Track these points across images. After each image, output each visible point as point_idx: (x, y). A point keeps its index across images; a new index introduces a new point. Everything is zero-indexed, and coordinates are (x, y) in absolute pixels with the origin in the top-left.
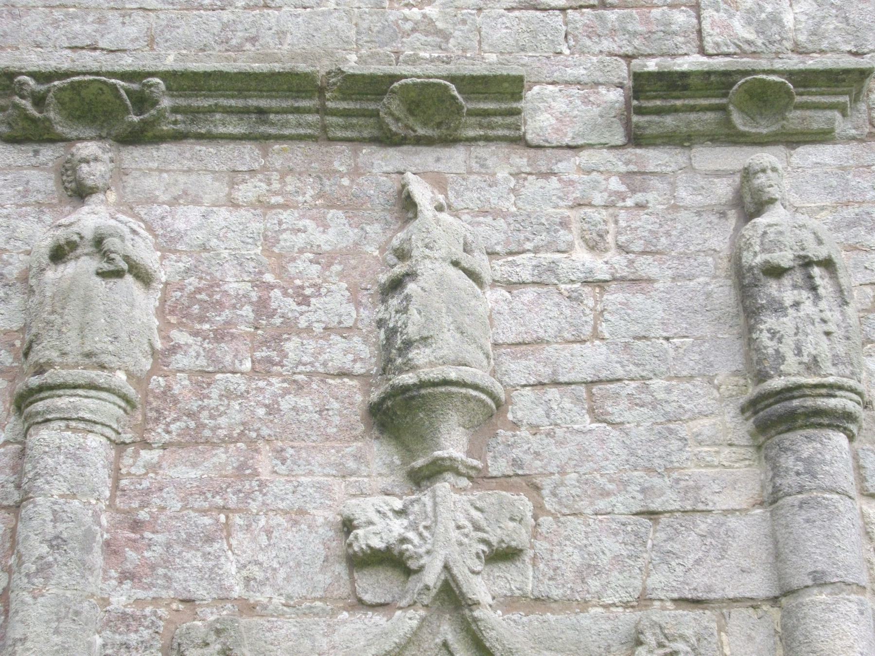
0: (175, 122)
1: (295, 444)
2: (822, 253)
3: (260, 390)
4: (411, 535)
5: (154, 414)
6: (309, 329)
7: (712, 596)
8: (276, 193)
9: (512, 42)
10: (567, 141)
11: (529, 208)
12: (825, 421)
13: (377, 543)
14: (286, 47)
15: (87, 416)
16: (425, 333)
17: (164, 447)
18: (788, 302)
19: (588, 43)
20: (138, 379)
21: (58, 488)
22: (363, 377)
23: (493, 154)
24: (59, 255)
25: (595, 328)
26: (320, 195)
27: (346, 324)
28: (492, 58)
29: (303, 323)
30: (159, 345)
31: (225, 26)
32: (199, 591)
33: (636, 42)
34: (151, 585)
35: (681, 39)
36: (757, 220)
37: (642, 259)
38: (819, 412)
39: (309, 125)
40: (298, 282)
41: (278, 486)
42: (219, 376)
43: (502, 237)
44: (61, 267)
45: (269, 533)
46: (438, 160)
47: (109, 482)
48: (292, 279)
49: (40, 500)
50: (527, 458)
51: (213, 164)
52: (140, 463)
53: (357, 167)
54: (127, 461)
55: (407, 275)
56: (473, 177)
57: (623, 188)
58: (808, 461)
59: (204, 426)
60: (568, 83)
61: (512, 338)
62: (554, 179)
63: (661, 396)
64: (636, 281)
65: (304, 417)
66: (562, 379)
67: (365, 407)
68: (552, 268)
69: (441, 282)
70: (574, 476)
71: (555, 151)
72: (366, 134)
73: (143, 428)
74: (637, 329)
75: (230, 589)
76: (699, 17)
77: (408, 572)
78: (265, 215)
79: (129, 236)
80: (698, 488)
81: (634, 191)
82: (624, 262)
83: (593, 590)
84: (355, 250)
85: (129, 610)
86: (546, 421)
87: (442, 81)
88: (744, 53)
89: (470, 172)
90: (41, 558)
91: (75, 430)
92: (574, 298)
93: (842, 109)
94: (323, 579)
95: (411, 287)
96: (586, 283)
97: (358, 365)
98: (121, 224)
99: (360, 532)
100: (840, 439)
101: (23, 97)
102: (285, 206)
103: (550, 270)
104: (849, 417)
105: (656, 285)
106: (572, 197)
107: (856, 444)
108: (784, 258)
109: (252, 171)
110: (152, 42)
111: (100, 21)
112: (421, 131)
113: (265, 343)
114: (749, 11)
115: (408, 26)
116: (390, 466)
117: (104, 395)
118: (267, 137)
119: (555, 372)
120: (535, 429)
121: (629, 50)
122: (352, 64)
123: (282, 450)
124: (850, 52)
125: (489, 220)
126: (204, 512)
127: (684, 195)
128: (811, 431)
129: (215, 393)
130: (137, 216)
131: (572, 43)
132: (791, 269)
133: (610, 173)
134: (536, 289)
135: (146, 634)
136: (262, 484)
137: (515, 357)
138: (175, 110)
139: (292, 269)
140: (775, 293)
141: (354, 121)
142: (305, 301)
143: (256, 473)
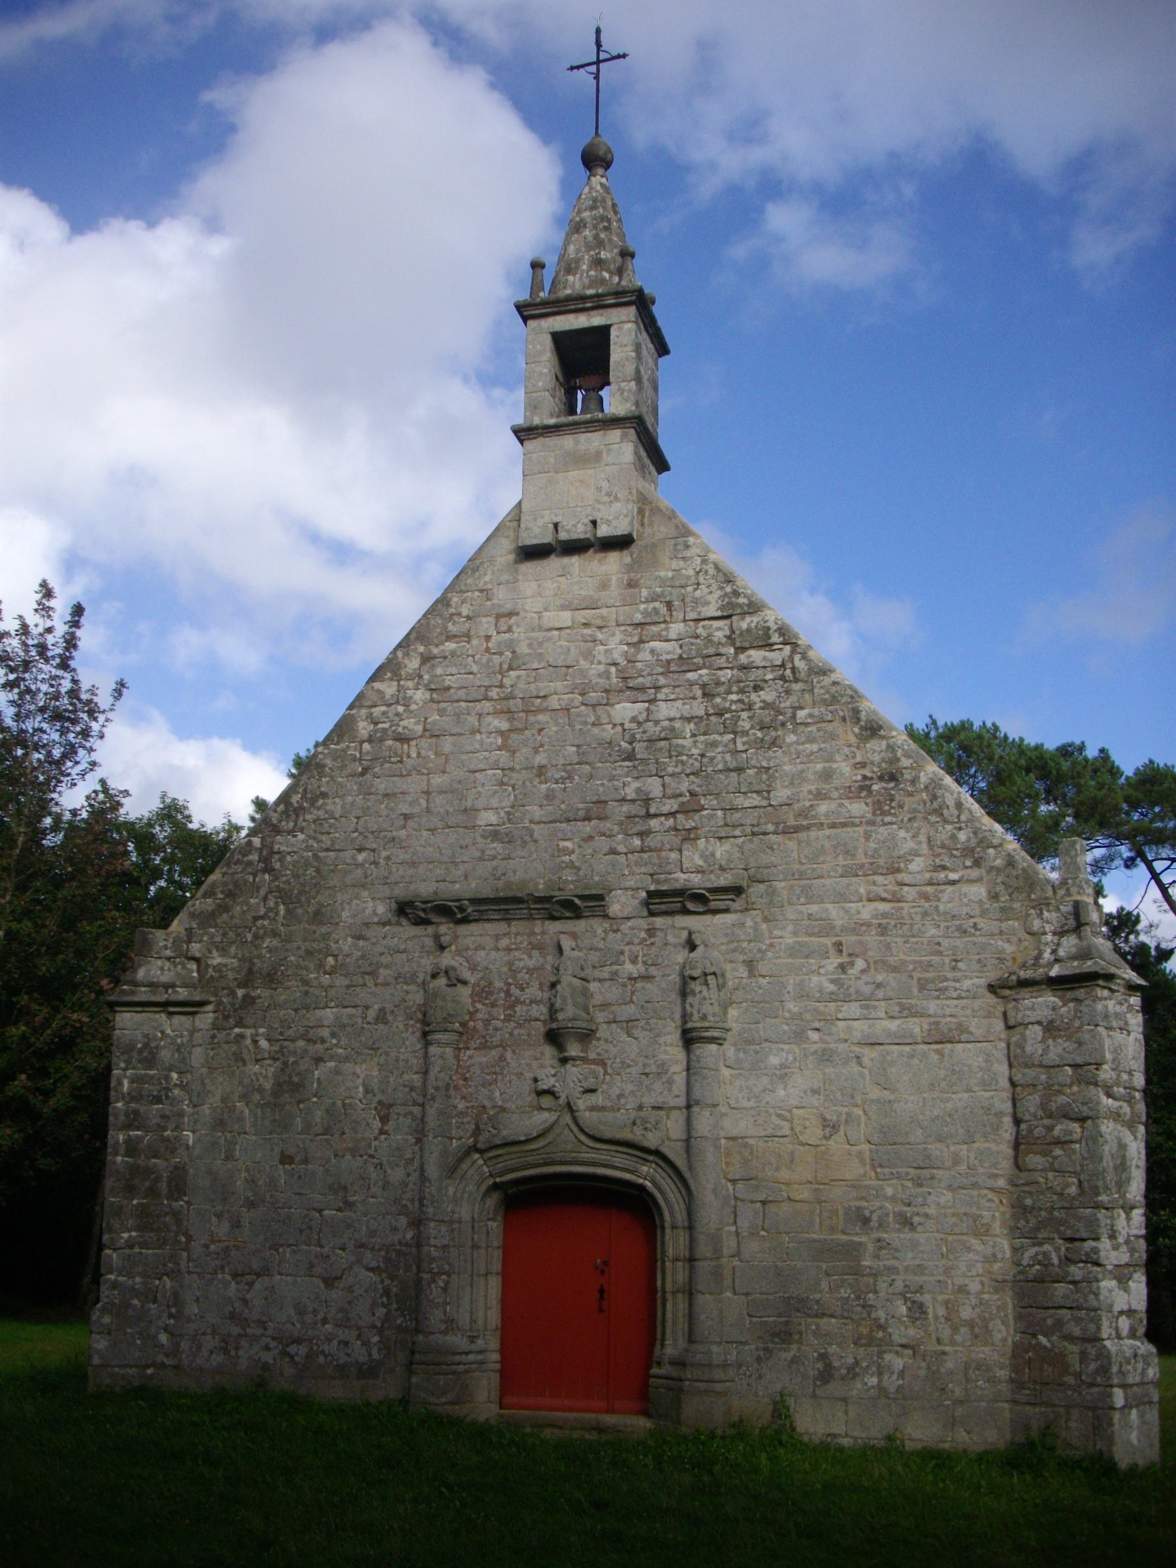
2: (712, 970)
13: (545, 1087)
21: (437, 1069)
22: (544, 1022)
24: (434, 976)
26: (530, 943)
28: (597, 878)
32: (487, 1103)
41: (514, 1064)
60: (626, 889)
61: (599, 1003)
64: (648, 978)
68: (615, 973)
69: (570, 985)
73: (466, 1042)
74: (646, 998)
84: (542, 968)
92: (624, 985)
93: (733, 900)
94: (529, 1099)
95: (559, 987)
102: (516, 949)
108: (696, 973)
109: (504, 935)
110: (466, 877)
111: (446, 869)
112: (568, 915)
116: (553, 1056)
120: (606, 1041)
127: (670, 939)
137: (600, 1011)
142: (523, 990)
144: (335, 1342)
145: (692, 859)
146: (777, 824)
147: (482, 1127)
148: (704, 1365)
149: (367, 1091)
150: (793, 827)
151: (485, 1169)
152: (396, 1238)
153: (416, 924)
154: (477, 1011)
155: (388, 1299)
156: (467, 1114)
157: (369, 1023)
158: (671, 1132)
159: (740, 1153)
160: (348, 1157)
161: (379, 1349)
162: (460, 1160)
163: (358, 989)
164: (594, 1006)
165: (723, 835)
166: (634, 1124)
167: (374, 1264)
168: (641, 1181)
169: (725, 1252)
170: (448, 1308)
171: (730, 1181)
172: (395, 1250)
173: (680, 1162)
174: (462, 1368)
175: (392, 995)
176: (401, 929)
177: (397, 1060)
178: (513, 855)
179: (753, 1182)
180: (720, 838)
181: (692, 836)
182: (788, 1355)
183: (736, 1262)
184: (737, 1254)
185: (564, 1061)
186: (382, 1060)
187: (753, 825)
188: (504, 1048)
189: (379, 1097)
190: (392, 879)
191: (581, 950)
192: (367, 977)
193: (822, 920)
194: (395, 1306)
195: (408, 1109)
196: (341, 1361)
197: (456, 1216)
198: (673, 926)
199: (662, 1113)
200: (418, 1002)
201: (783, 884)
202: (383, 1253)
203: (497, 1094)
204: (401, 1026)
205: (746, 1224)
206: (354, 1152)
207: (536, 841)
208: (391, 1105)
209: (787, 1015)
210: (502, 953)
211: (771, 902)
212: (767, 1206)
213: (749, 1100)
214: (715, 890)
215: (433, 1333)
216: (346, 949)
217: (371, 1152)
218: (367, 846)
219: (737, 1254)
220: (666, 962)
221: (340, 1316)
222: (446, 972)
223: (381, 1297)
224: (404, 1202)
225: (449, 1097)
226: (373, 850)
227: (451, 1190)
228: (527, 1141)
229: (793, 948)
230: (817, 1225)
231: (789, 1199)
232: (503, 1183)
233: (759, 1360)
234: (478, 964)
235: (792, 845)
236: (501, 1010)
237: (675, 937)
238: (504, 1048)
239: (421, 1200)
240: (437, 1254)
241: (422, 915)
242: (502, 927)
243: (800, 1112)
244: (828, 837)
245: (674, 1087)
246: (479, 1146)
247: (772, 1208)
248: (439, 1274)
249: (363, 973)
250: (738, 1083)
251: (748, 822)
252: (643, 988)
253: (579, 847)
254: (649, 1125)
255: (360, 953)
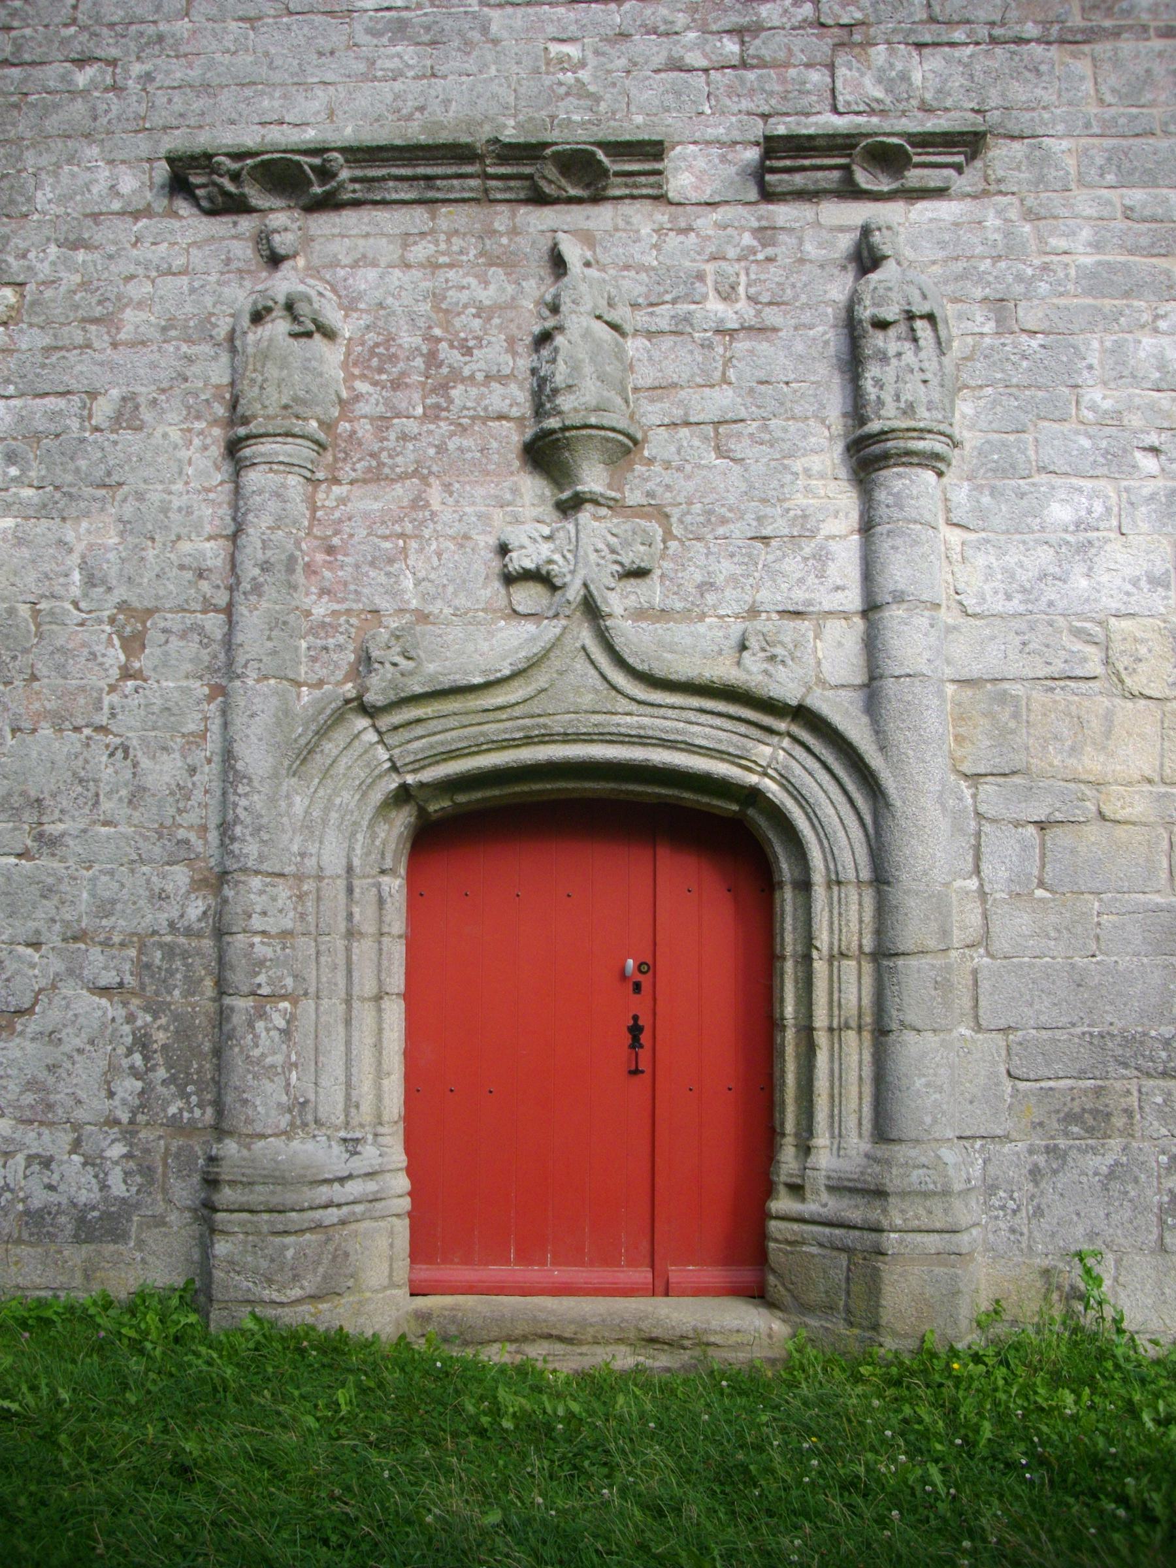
0: (354, 191)
1: (461, 479)
2: (925, 308)
3: (430, 432)
4: (557, 557)
5: (342, 455)
6: (472, 377)
7: (811, 609)
8: (443, 254)
9: (657, 103)
10: (705, 197)
11: (669, 262)
12: (915, 460)
13: (529, 565)
14: (451, 114)
15: (286, 460)
16: (570, 382)
17: (351, 483)
18: (891, 352)
19: (728, 103)
20: (327, 426)
21: (266, 521)
22: (520, 420)
23: (638, 211)
24: (257, 317)
25: (724, 373)
26: (482, 254)
27: (504, 373)
28: (639, 119)
29: (466, 372)
30: (345, 395)
31: (397, 97)
32: (383, 603)
33: (773, 102)
34: (344, 600)
35: (815, 98)
36: (871, 276)
37: (767, 310)
38: (909, 453)
39: (472, 189)
40: (462, 335)
41: (447, 515)
42: (396, 421)
43: (644, 289)
44: (260, 330)
45: (439, 555)
46: (588, 218)
47: (308, 513)
48: (457, 333)
49: (251, 531)
50: (660, 490)
51: (389, 229)
52: (332, 496)
53: (515, 227)
54: (321, 495)
55: (556, 328)
56: (618, 234)
57: (755, 243)
58: (897, 495)
59: (384, 464)
60: (708, 143)
61: (649, 382)
62: (693, 234)
63: (779, 434)
64: (761, 330)
65: (468, 456)
66: (692, 420)
67: (520, 446)
68: (687, 319)
69: (587, 334)
70: (699, 505)
71: (694, 208)
72: (522, 196)
73: (332, 468)
74: (762, 375)
75: (408, 602)
76: (833, 76)
77: (554, 588)
78: (433, 274)
79: (315, 298)
80: (805, 517)
81: (764, 246)
82: (752, 312)
83: (710, 603)
85: (327, 620)
86: (677, 458)
87: (589, 147)
88: (872, 112)
89: (617, 229)
90: (254, 579)
91: (276, 472)
92: (707, 346)
93: (959, 168)
94: (488, 592)
95: (559, 340)
96: (717, 332)
97: (514, 409)
98: (312, 287)
99: (514, 555)
100: (929, 476)
101: (221, 176)
102: (451, 266)
103: (686, 319)
104: (937, 457)
105: (780, 334)
106: (708, 251)
107: (945, 480)
108: (890, 313)
109: (422, 234)
110: (331, 115)
111: (284, 96)
112: (573, 192)
113: (433, 390)
114: (881, 70)
115: (562, 90)
116: (542, 497)
117: (299, 441)
118: (436, 201)
119: (686, 414)
120: (667, 465)
121: (766, 109)
122: (510, 133)
123: (450, 484)
124: (973, 110)
125: (632, 273)
126: (385, 538)
128: (901, 469)
129: (392, 436)
130: (322, 279)
131: (713, 102)
132: (895, 322)
133: (742, 229)
134: (673, 338)
135: (341, 639)
136: (433, 514)
137: (652, 401)
138: (354, 180)
139: (458, 322)
140: (881, 344)
141: (512, 183)
142: (468, 352)
143: (427, 505)
144: (20, 1158)
145: (860, 85)
146: (1046, 24)
147: (375, 653)
148: (926, 1195)
149: (90, 581)
150: (1083, 31)
151: (382, 754)
152: (163, 918)
153: (211, 213)
154: (358, 398)
155: (146, 1058)
156: (335, 627)
157: (97, 429)
158: (826, 667)
159: (989, 714)
160: (46, 731)
161: (127, 1174)
162: (323, 732)
163: (73, 356)
164: (636, 389)
165: (928, 38)
166: (743, 647)
167: (108, 978)
168: (753, 779)
169: (957, 937)
170: (294, 1075)
171: (966, 776)
172: (161, 946)
173: (857, 731)
174: (332, 1216)
175: (153, 366)
176: (176, 224)
177: (165, 510)
178: (442, 69)
179: (1017, 780)
180: (919, 46)
181: (857, 38)
182: (1102, 1163)
183: (980, 959)
184: (985, 939)
185: (569, 507)
186: (128, 511)
187: (992, 24)
188: (424, 479)
189: (121, 593)
190: (157, 120)
191: (603, 268)
192: (93, 328)
193: (1154, 220)
194: (162, 1073)
195: (189, 619)
196: (36, 1203)
197: (310, 863)
198: (818, 224)
199: (805, 625)
200: (215, 380)
201: (1065, 144)
202: (133, 953)
203: (408, 583)
204: (175, 435)
205: (1003, 874)
206: (60, 721)
207: (495, 42)
208: (150, 612)
209: (1089, 416)
210: (416, 274)
211: (1040, 180)
212: (1050, 833)
213: (1009, 597)
214: (925, 141)
215: (263, 1136)
216: (44, 270)
217: (102, 719)
218: (99, 53)
219: (985, 939)
220: (803, 298)
221: (29, 1098)
222: (289, 307)
223: (130, 1052)
224: (181, 834)
225: (294, 587)
226: (113, 63)
227: (299, 803)
228: (487, 685)
229: (1094, 275)
230: (1164, 875)
231: (1102, 816)
232: (422, 785)
233: (1035, 1174)
234: (360, 297)
235: (1082, 67)
236: (416, 396)
237: (820, 246)
238: (424, 479)
239: (225, 828)
240: (268, 952)
241: (231, 187)
242: (418, 217)
243: (1125, 624)
244: (1160, 55)
245: (832, 569)
246: (370, 698)
247: (1060, 837)
248: (274, 997)
249: (84, 320)
250: (981, 560)
251: (982, 15)
252: (751, 352)
253: (597, 53)
254: (779, 651)
255: (77, 278)
